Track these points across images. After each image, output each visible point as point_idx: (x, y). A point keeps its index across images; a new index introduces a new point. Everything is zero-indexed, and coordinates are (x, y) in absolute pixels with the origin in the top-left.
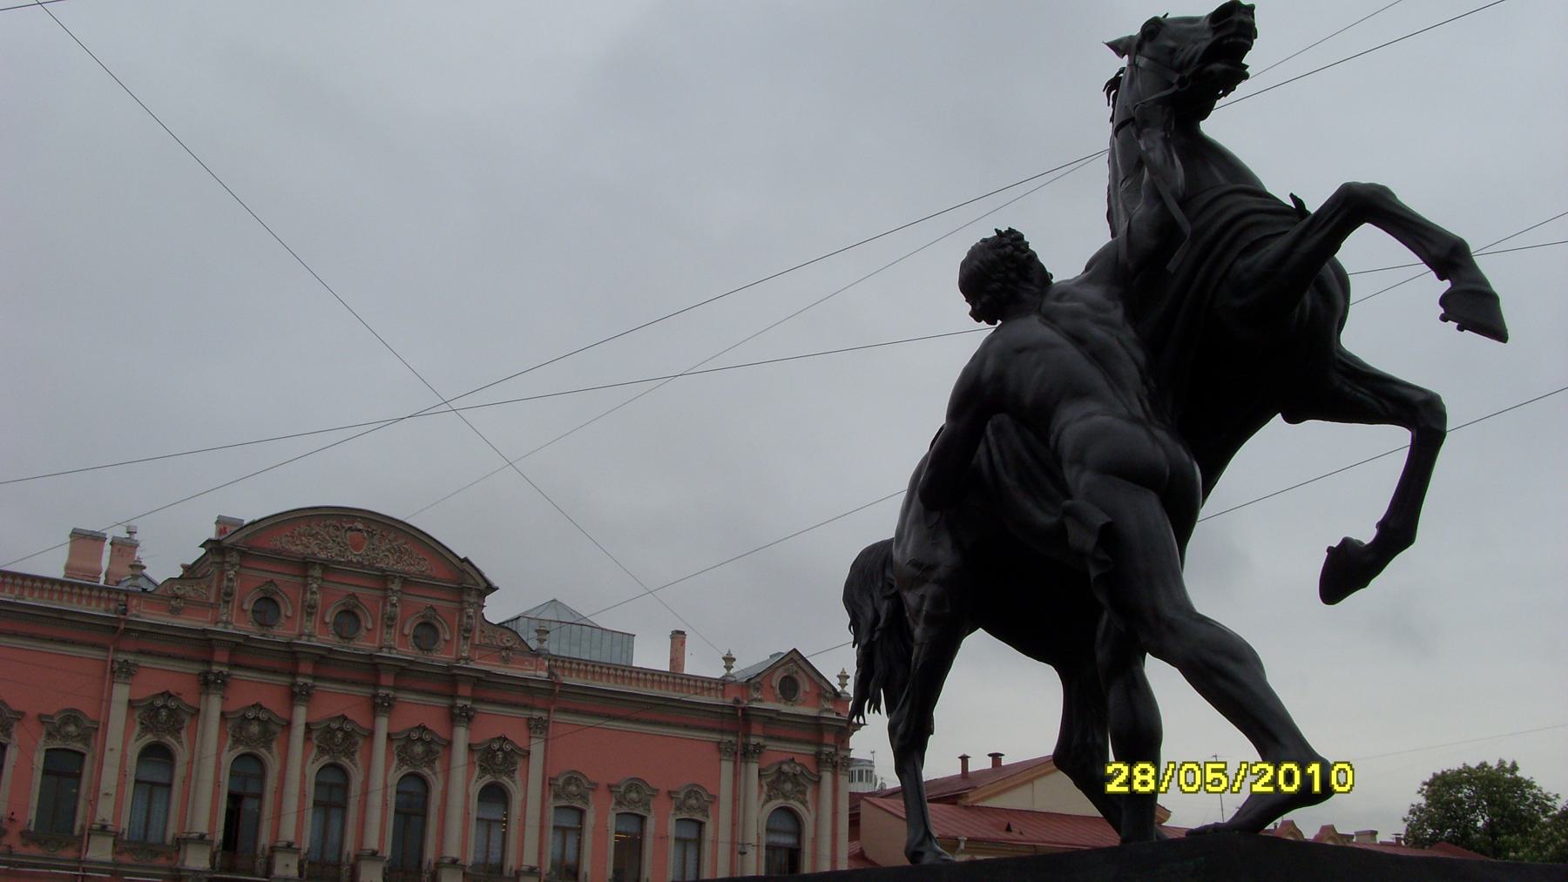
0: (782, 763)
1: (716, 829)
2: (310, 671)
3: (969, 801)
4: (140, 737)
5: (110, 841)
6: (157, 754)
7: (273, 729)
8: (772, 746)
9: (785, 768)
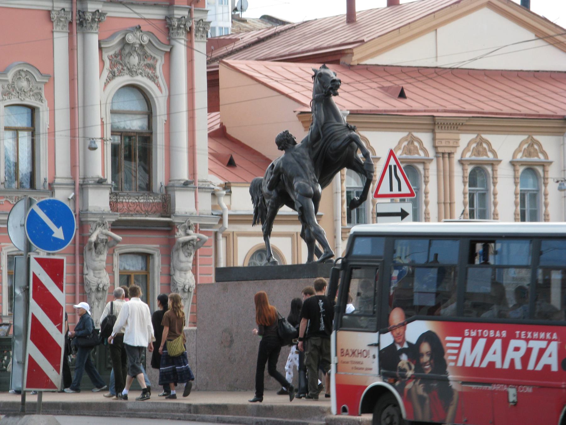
0: (127, 32)
1: (52, 111)
3: (355, 59)
7: (494, 338)
9: (130, 38)
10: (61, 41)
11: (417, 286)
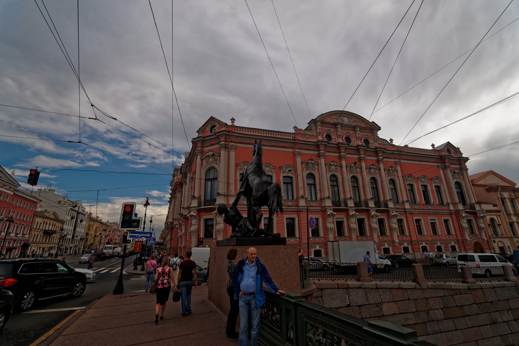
2: (363, 153)
4: (306, 172)
5: (304, 200)
6: (311, 176)
8: (452, 166)
10: (441, 172)
11: (349, 205)
